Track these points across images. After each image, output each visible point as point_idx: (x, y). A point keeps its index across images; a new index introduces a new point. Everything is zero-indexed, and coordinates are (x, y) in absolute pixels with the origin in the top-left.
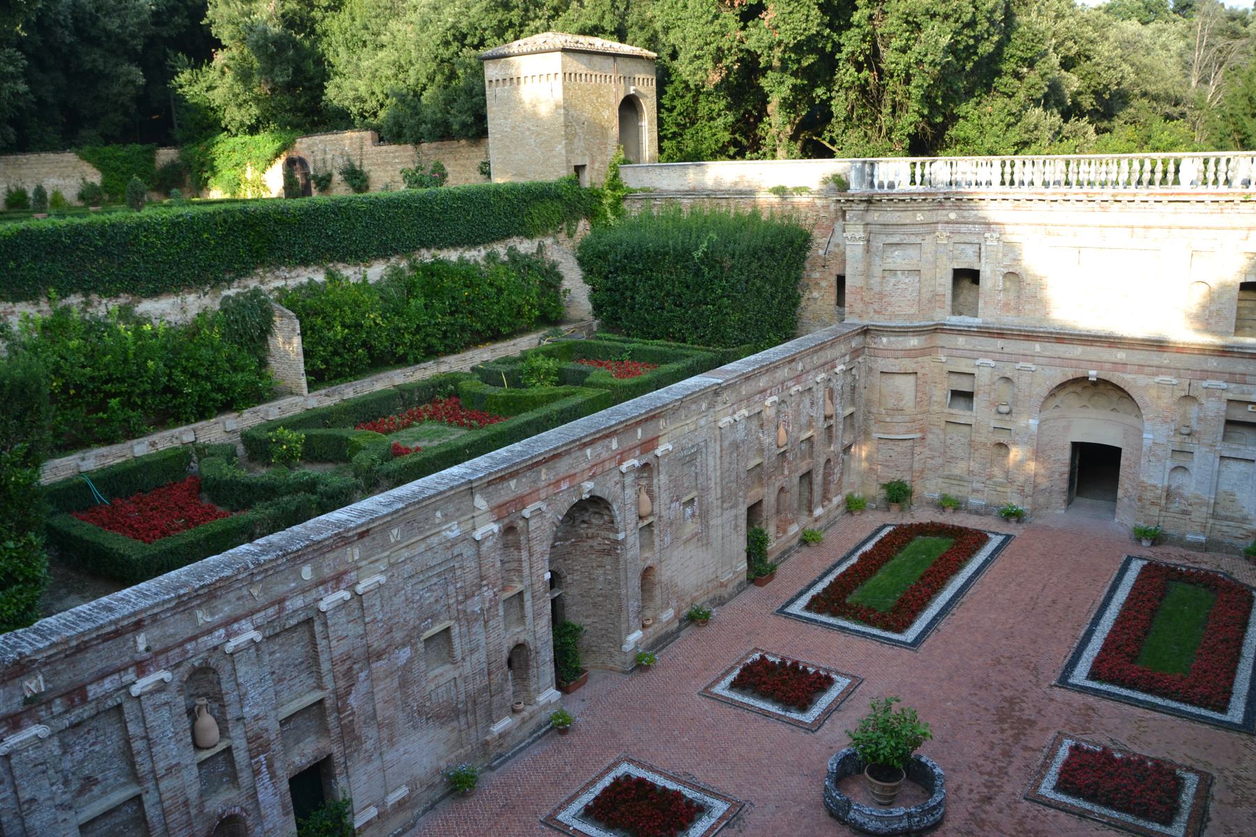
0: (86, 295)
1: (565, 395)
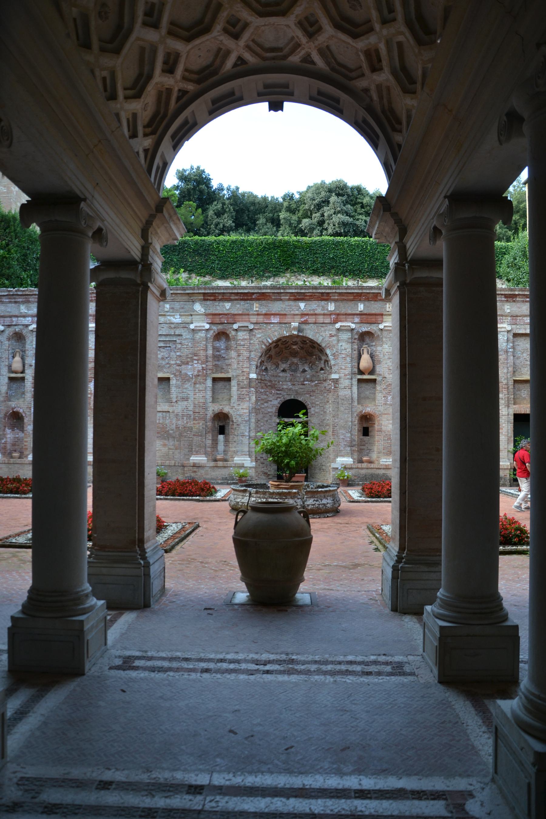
0: (190, 274)
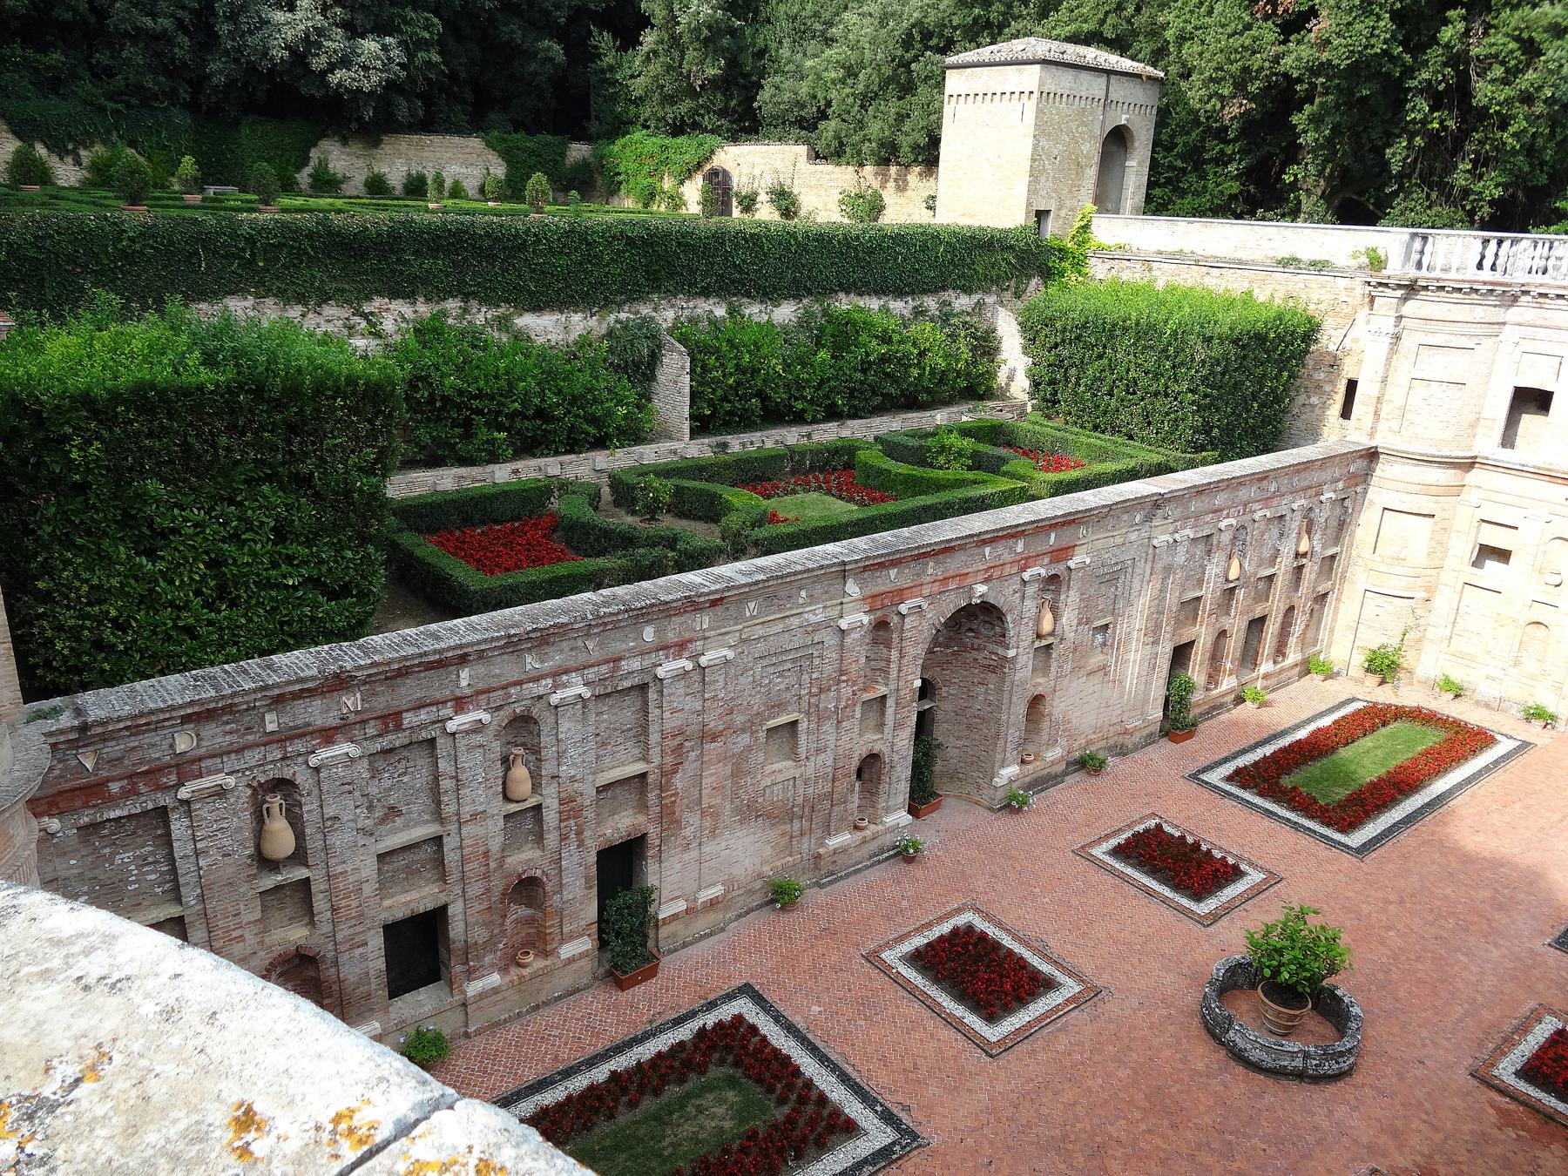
1: (975, 482)
